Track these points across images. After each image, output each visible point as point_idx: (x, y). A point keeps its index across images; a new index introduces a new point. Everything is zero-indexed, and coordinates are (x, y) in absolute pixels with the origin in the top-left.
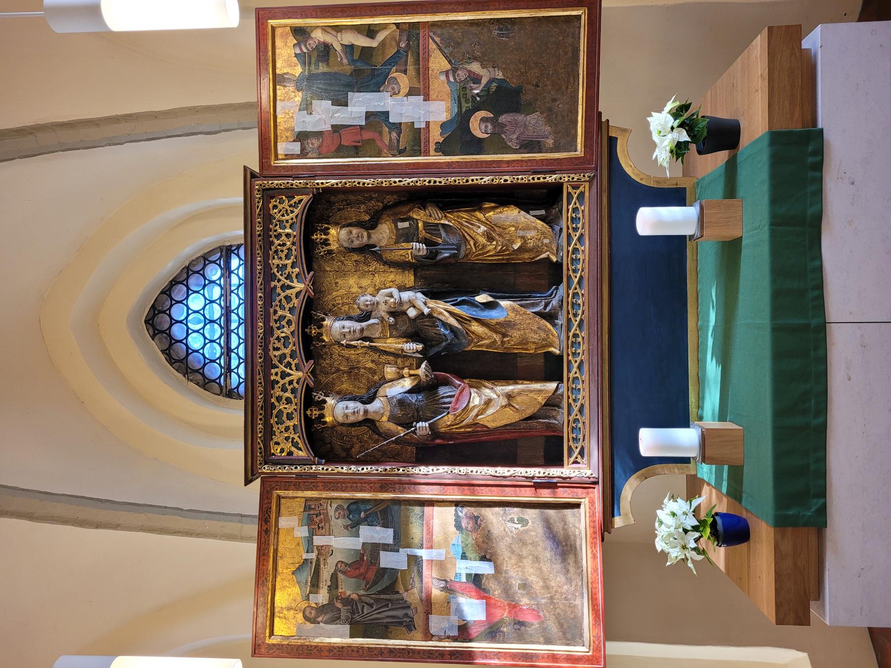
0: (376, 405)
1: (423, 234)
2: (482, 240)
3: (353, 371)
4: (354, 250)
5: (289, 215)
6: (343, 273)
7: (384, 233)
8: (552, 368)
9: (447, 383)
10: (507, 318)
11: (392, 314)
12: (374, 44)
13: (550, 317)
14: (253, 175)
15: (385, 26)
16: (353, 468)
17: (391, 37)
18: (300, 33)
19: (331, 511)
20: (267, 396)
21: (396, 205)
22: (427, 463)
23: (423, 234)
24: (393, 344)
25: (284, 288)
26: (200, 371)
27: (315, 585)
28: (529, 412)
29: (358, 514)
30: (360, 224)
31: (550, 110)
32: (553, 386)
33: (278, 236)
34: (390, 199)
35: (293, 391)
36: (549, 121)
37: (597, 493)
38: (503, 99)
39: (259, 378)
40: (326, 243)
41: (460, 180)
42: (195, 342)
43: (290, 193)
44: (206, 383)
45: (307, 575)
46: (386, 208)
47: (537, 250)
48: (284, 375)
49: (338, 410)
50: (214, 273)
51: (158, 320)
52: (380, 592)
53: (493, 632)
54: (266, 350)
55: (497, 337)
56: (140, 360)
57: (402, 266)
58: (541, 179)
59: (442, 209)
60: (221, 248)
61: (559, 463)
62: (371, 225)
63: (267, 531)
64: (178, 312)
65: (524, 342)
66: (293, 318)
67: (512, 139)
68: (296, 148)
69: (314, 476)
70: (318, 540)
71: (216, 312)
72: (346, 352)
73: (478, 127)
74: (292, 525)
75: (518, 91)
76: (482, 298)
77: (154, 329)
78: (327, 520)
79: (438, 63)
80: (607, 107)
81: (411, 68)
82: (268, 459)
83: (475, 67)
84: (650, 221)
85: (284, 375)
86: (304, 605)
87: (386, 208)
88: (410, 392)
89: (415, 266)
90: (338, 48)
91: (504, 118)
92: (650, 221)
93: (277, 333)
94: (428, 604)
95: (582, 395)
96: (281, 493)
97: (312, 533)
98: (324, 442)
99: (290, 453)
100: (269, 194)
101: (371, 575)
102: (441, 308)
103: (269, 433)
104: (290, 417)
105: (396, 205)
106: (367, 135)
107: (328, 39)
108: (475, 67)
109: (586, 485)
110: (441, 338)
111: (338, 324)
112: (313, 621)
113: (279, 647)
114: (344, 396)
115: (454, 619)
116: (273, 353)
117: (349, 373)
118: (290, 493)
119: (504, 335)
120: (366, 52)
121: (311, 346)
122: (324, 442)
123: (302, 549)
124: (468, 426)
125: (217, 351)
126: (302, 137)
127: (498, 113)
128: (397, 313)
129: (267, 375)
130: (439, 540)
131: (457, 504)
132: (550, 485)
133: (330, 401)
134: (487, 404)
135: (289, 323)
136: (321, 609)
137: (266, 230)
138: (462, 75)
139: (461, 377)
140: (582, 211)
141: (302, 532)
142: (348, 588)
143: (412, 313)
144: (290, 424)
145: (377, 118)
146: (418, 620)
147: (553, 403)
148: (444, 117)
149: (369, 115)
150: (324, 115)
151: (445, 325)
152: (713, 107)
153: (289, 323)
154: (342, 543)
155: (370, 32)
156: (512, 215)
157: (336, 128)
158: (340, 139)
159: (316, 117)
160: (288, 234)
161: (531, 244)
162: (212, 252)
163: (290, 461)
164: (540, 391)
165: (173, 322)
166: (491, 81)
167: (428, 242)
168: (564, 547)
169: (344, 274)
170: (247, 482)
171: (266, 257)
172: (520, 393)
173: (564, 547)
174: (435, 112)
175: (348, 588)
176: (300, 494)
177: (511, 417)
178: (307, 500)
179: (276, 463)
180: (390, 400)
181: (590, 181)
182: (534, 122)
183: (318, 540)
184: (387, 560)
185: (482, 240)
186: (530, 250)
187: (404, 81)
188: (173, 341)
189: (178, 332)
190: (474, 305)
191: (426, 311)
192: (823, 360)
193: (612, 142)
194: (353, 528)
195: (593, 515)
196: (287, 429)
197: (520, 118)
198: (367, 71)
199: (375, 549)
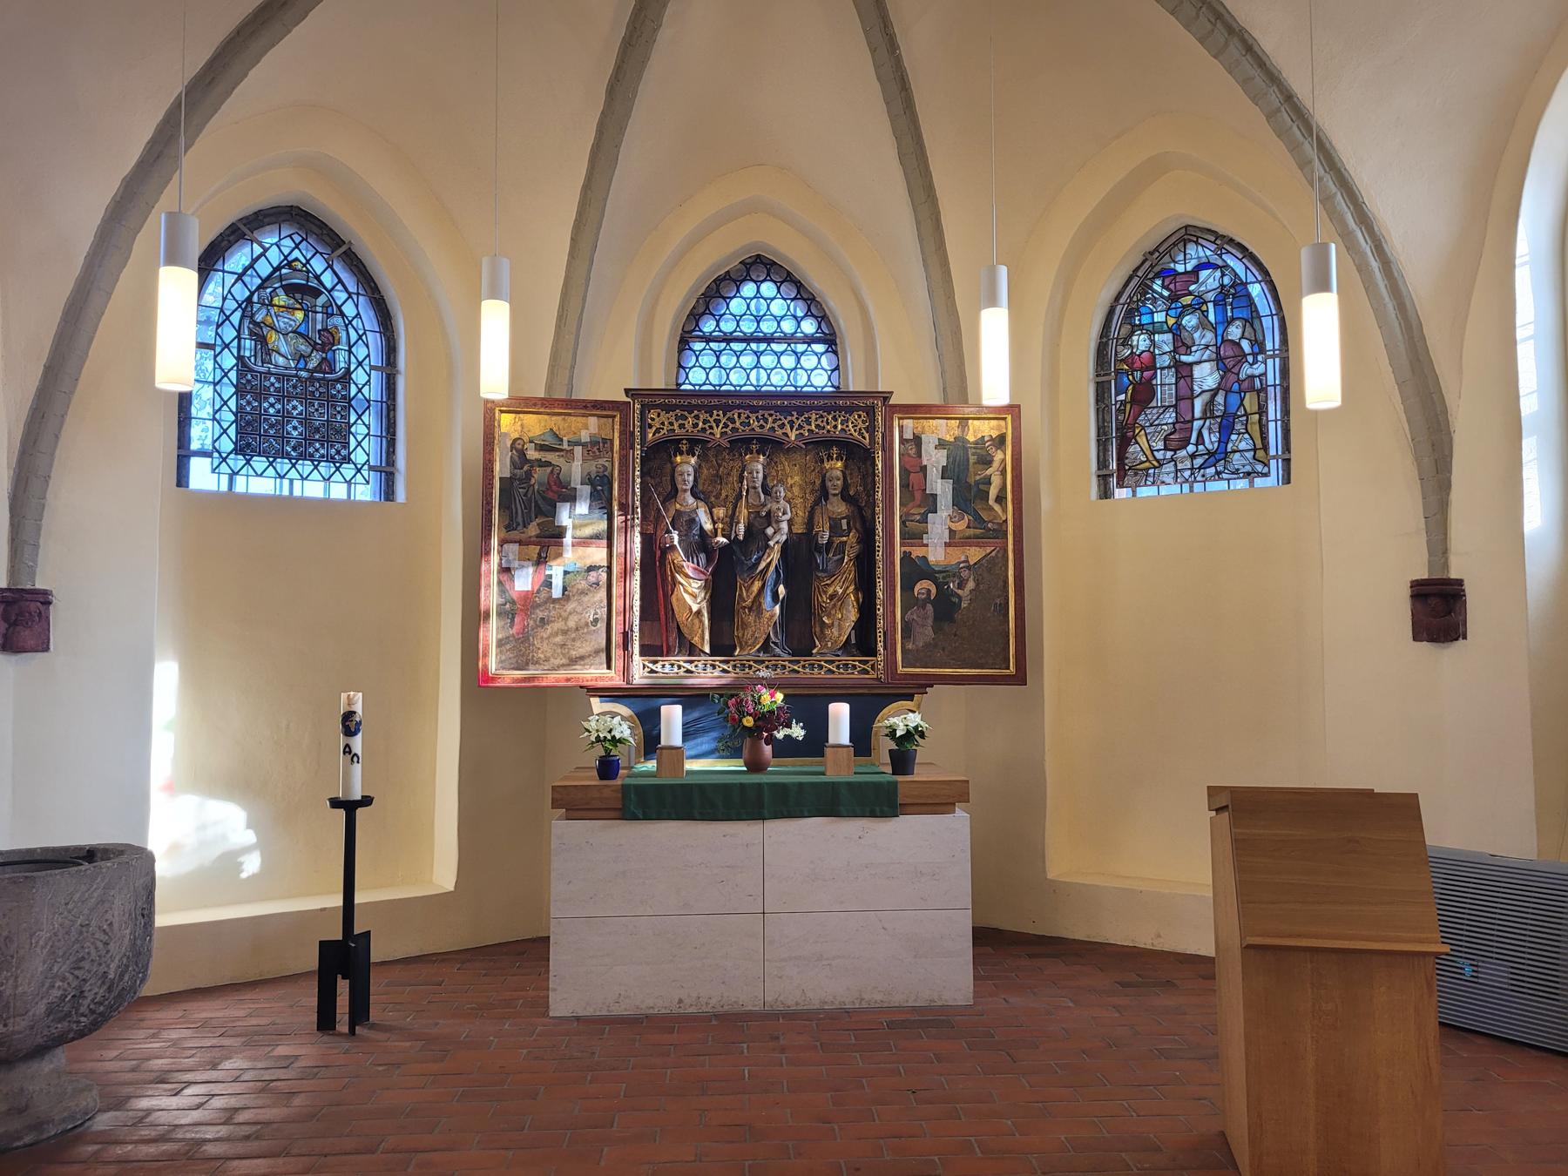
0: (691, 500)
1: (837, 540)
2: (831, 590)
3: (718, 479)
4: (823, 481)
5: (853, 427)
6: (803, 471)
7: (839, 508)
9: (709, 561)
10: (768, 610)
11: (769, 513)
12: (991, 502)
13: (765, 647)
14: (886, 399)
15: (1005, 510)
16: (638, 481)
17: (996, 516)
18: (1000, 441)
19: (601, 461)
20: (699, 407)
21: (862, 517)
22: (643, 543)
23: (837, 540)
24: (743, 513)
25: (791, 423)
26: (707, 311)
27: (542, 448)
28: (685, 631)
30: (846, 487)
31: (936, 646)
32: (707, 649)
33: (835, 419)
34: (867, 513)
35: (704, 430)
36: (927, 645)
37: (618, 682)
38: (945, 607)
39: (715, 402)
40: (830, 458)
41: (879, 571)
42: (736, 306)
43: (871, 429)
44: (695, 316)
45: (550, 441)
46: (860, 509)
47: (822, 637)
48: (717, 422)
49: (687, 466)
50: (809, 327)
51: (759, 266)
52: (537, 505)
54: (739, 407)
55: (749, 602)
57: (810, 523)
58: (880, 639)
59: (857, 557)
60: (833, 334)
61: (642, 654)
62: (845, 496)
63: (585, 407)
64: (768, 289)
65: (744, 626)
66: (765, 431)
67: (913, 615)
68: (908, 435)
69: (632, 447)
70: (578, 450)
71: (768, 327)
72: (735, 473)
73: (922, 586)
74: (591, 427)
75: (952, 620)
76: (782, 589)
77: (752, 264)
78: (595, 458)
79: (975, 554)
80: (936, 691)
81: (971, 532)
82: (645, 408)
83: (971, 585)
84: (840, 713)
85: (717, 422)
86: (526, 439)
87: (860, 509)
88: (701, 527)
89: (809, 535)
90: (988, 472)
91: (929, 607)
92: (840, 713)
93: (753, 416)
96: (617, 419)
97: (584, 445)
98: (659, 456)
99: (650, 426)
100: (870, 411)
101: (550, 495)
102: (774, 556)
103: (668, 408)
104: (682, 426)
105: (862, 517)
106: (918, 495)
107: (996, 464)
108: (971, 585)
109: (626, 670)
110: (748, 555)
111: (760, 467)
112: (512, 447)
113: (493, 418)
114: (697, 471)
115: (516, 564)
116: (736, 412)
117: (717, 475)
118: (617, 427)
119: (750, 609)
120: (985, 495)
121: (742, 444)
122: (659, 456)
123: (572, 437)
124: (674, 578)
125: (728, 326)
126: (917, 440)
127: (933, 603)
128: (769, 519)
129: (717, 408)
131: (609, 568)
133: (693, 460)
134: (691, 593)
135: (762, 427)
136: (522, 453)
137: (840, 409)
138: (965, 574)
139: (713, 574)
140: (854, 671)
141: (585, 436)
142: (539, 475)
143: (770, 531)
144: (676, 426)
145: (931, 503)
146: (514, 534)
148: (931, 559)
149: (934, 496)
150: (935, 459)
151: (759, 560)
152: (923, 752)
153: (762, 427)
154: (576, 470)
155: (1001, 499)
156: (852, 615)
157: (924, 469)
158: (915, 471)
159: (933, 452)
160: (837, 426)
161: (828, 632)
162: (829, 324)
163: (645, 426)
164: (703, 638)
165: (758, 283)
166: (960, 597)
167: (830, 543)
169: (803, 472)
170: (627, 391)
171: (818, 408)
172: (701, 621)
174: (936, 552)
175: (539, 475)
176: (617, 435)
177: (682, 616)
178: (612, 441)
179: (642, 413)
180: (695, 511)
181: (878, 679)
182: (926, 633)
183: (578, 450)
185: (831, 590)
186: (822, 631)
187: (960, 526)
188: (738, 283)
189: (748, 289)
190: (776, 584)
191: (771, 543)
192: (739, 818)
193: (910, 697)
194: (589, 480)
195: (602, 679)
196: (671, 424)
197: (930, 621)
198: (969, 496)
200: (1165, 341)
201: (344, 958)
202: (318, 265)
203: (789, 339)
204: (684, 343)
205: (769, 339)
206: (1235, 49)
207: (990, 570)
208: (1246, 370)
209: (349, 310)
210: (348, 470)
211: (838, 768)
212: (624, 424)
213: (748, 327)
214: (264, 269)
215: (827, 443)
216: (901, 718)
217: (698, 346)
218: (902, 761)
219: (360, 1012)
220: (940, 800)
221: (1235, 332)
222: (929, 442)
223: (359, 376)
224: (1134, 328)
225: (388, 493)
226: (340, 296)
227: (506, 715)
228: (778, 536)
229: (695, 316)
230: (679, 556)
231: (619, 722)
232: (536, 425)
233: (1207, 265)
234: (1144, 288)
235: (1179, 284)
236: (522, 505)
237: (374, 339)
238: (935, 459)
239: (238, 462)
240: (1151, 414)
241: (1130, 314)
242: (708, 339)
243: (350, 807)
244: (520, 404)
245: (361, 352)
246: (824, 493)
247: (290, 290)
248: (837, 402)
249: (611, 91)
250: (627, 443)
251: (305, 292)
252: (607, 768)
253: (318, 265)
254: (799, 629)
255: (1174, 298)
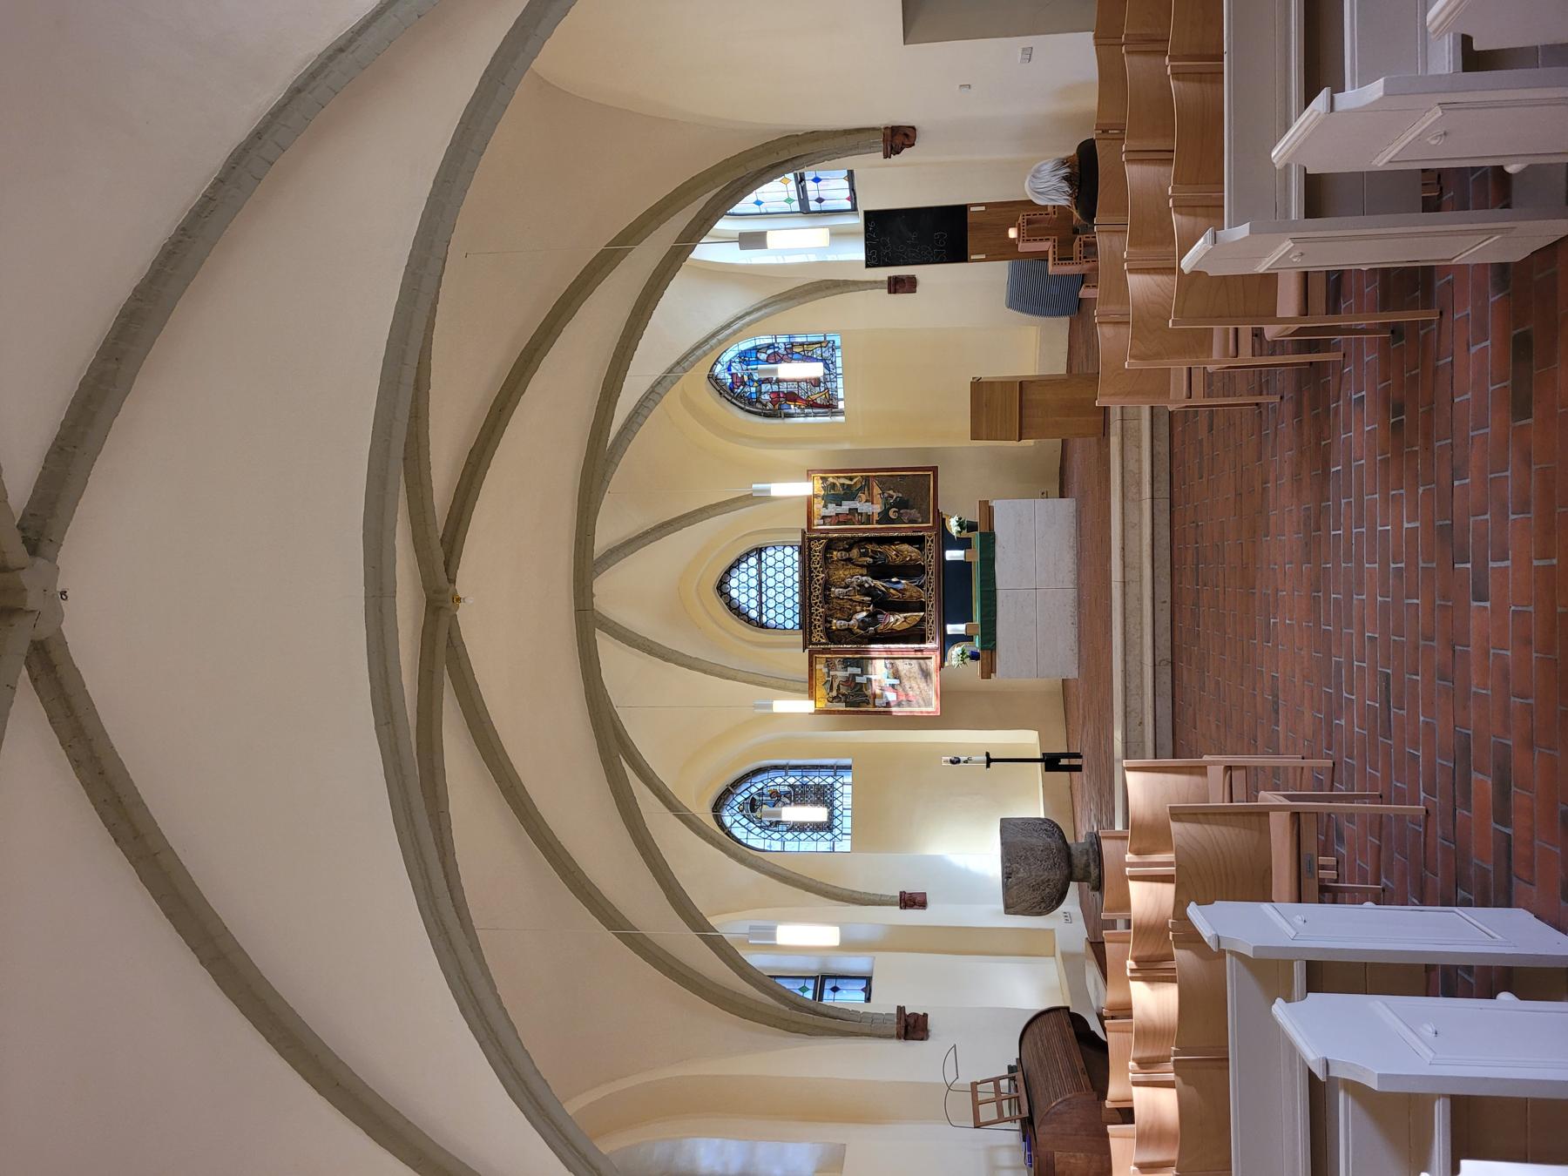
3: (842, 609)
5: (818, 547)
7: (855, 553)
8: (921, 607)
13: (921, 587)
26: (746, 614)
29: (847, 663)
38: (901, 504)
42: (743, 599)
43: (819, 539)
44: (749, 620)
49: (837, 624)
50: (753, 561)
51: (722, 588)
53: (899, 704)
56: (718, 606)
57: (862, 566)
62: (848, 550)
64: (734, 583)
71: (753, 583)
73: (892, 514)
74: (821, 668)
79: (877, 491)
84: (953, 555)
92: (953, 555)
94: (875, 696)
95: (933, 614)
98: (833, 636)
100: (810, 540)
102: (878, 583)
109: (933, 650)
121: (827, 599)
122: (833, 636)
125: (753, 604)
126: (823, 517)
130: (879, 673)
132: (921, 651)
134: (896, 621)
142: (843, 690)
145: (853, 511)
147: (923, 620)
150: (832, 509)
154: (841, 674)
156: (906, 547)
160: (817, 557)
168: (926, 674)
173: (926, 674)
174: (877, 508)
177: (906, 626)
184: (858, 679)
187: (864, 497)
188: (731, 599)
189: (734, 593)
194: (845, 668)
198: (849, 493)
199: (854, 675)
200: (765, 387)
201: (1051, 762)
202: (740, 799)
203: (760, 573)
204: (763, 626)
205: (760, 583)
206: (659, 389)
207: (884, 483)
208: (782, 351)
209: (760, 786)
210: (837, 785)
211: (975, 556)
212: (819, 652)
213: (753, 593)
214: (744, 822)
215: (826, 558)
216: (953, 526)
217: (764, 619)
218: (972, 527)
219: (1078, 756)
220: (987, 511)
221: (763, 356)
222: (825, 512)
223: (791, 781)
224: (758, 400)
225: (848, 768)
226: (753, 790)
227: (956, 708)
228: (869, 581)
229: (749, 620)
230: (880, 627)
231: (955, 651)
232: (821, 692)
233: (729, 369)
234: (740, 397)
235: (738, 381)
236: (855, 700)
237: (772, 774)
238: (832, 509)
239: (836, 831)
240: (801, 393)
241: (750, 404)
242: (761, 614)
243: (989, 761)
244: (812, 696)
245: (779, 780)
246: (849, 560)
247: (753, 810)
248: (805, 551)
249: (667, 660)
250: (824, 651)
251: (753, 805)
252: (974, 656)
253: (740, 799)
254: (912, 571)
255: (744, 384)
